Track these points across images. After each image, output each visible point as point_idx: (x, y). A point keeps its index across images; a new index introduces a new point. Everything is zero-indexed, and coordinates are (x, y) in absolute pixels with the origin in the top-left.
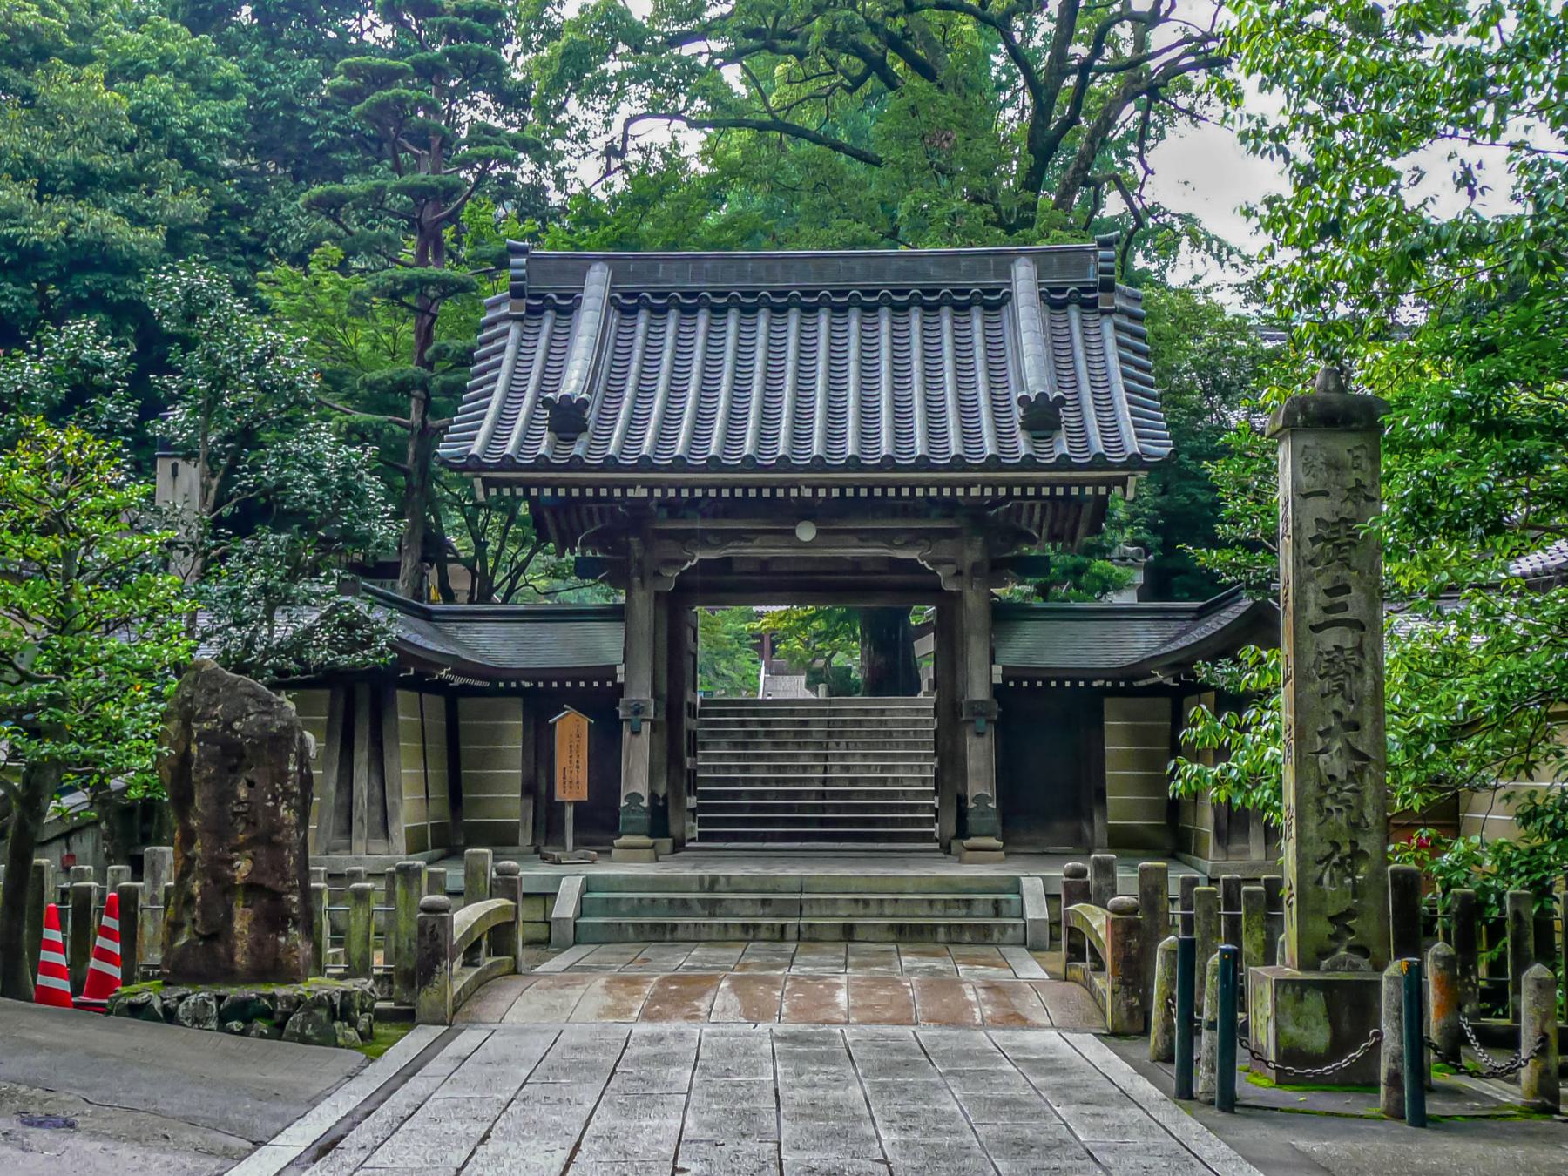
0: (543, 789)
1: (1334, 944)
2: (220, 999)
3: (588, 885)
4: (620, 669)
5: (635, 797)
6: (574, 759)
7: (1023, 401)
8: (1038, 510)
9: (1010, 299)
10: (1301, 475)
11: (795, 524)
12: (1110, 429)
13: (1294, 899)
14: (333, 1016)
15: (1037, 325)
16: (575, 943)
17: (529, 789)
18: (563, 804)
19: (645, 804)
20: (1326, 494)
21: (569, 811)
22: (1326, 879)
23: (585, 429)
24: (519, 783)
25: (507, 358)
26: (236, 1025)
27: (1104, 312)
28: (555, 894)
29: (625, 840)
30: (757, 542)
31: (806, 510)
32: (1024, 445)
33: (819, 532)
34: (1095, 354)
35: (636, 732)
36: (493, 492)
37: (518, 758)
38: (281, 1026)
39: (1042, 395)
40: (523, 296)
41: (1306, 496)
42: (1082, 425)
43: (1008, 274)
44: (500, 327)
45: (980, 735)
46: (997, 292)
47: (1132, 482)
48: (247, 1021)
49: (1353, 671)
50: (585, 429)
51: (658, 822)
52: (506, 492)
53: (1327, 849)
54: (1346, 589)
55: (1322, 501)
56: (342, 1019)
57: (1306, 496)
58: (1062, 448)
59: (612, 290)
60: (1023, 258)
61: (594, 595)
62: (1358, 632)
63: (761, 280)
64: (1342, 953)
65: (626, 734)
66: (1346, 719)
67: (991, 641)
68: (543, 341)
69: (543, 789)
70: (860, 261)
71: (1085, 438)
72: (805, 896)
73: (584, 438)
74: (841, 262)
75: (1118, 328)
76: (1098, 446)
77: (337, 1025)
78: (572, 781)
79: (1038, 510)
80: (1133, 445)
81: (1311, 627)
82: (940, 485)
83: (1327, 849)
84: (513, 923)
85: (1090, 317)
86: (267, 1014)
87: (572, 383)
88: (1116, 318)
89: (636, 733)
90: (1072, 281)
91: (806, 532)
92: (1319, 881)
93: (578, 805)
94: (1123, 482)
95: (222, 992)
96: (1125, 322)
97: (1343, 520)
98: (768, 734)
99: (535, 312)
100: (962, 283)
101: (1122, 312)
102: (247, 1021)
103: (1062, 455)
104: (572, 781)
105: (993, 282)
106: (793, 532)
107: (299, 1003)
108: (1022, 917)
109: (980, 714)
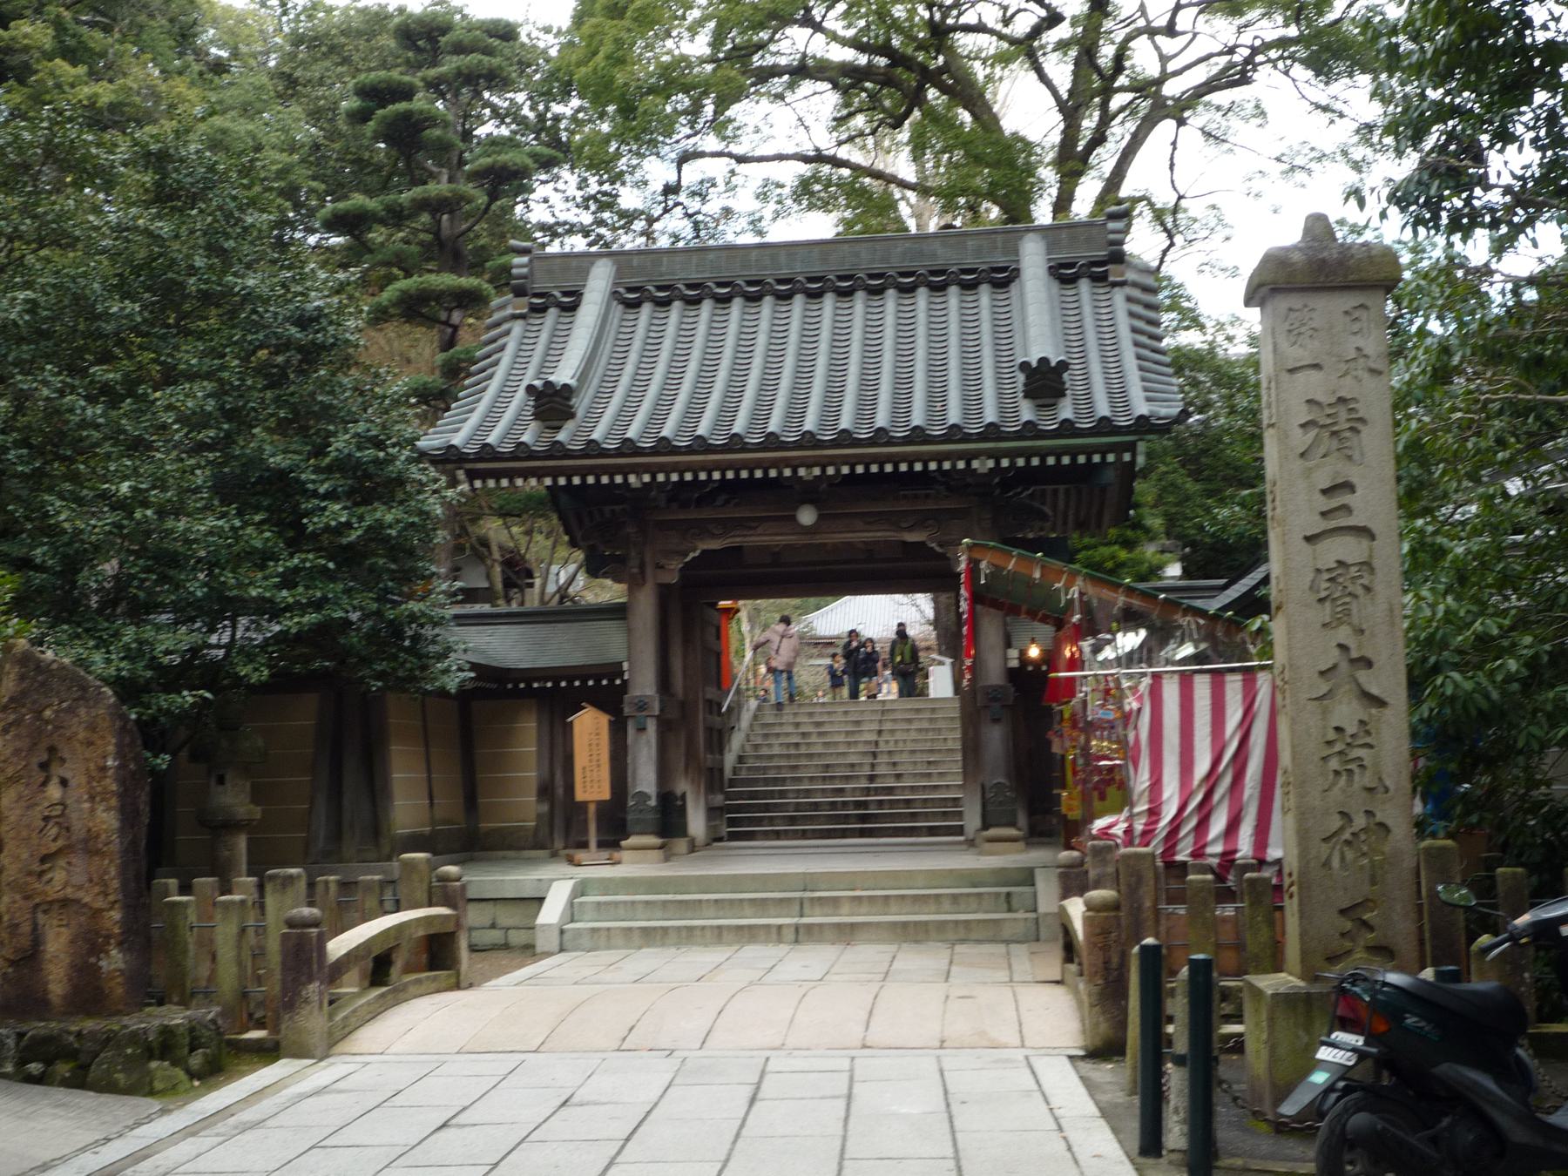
0: (560, 791)
1: (1348, 944)
2: (21, 1035)
3: (581, 889)
4: (625, 666)
5: (643, 796)
6: (595, 757)
7: (1025, 366)
8: (1061, 496)
9: (1018, 276)
10: (1284, 345)
11: (796, 509)
12: (1119, 395)
13: (1294, 889)
14: (150, 1053)
15: (1043, 295)
16: (562, 950)
17: (545, 791)
18: (585, 804)
19: (653, 803)
20: (1316, 366)
21: (592, 808)
22: (1336, 863)
23: (572, 416)
24: (533, 787)
25: (506, 358)
26: (35, 1067)
27: (1115, 285)
28: (541, 900)
29: (633, 840)
30: (759, 530)
31: (810, 493)
32: (1027, 412)
33: (821, 517)
34: (1106, 326)
35: (642, 729)
36: (478, 484)
37: (533, 761)
38: (85, 1068)
39: (1043, 361)
40: (524, 295)
41: (1292, 371)
42: (1088, 392)
43: (1016, 252)
44: (505, 327)
45: (996, 721)
46: (1004, 269)
47: (1141, 447)
48: (48, 1062)
49: (1360, 591)
50: (572, 416)
51: (668, 822)
52: (491, 483)
53: (1336, 822)
54: (1348, 487)
55: (1314, 375)
56: (162, 1058)
57: (1292, 371)
58: (1066, 411)
59: (615, 284)
60: (1031, 235)
61: (609, 591)
62: (1365, 543)
63: (765, 268)
64: (1359, 955)
65: (631, 731)
66: (1354, 654)
67: (1005, 625)
68: (544, 337)
69: (560, 791)
70: (865, 245)
71: (1090, 403)
72: (808, 894)
73: (570, 426)
74: (846, 247)
75: (1129, 299)
76: (1103, 409)
77: (154, 1064)
78: (592, 785)
79: (1061, 496)
80: (1142, 408)
81: (1309, 539)
82: (1012, 454)
83: (1336, 822)
84: (453, 933)
85: (1102, 291)
86: (70, 1054)
87: (564, 375)
88: (1128, 290)
89: (642, 729)
90: (1083, 254)
91: (807, 516)
92: (1327, 864)
93: (600, 803)
94: (1131, 448)
95: (24, 1028)
96: (1137, 293)
97: (1342, 400)
98: (820, 734)
99: (540, 310)
100: (969, 262)
101: (1135, 285)
102: (48, 1062)
103: (1066, 420)
104: (592, 785)
105: (1000, 260)
106: (793, 518)
107: (108, 1040)
108: (1035, 910)
109: (994, 699)
